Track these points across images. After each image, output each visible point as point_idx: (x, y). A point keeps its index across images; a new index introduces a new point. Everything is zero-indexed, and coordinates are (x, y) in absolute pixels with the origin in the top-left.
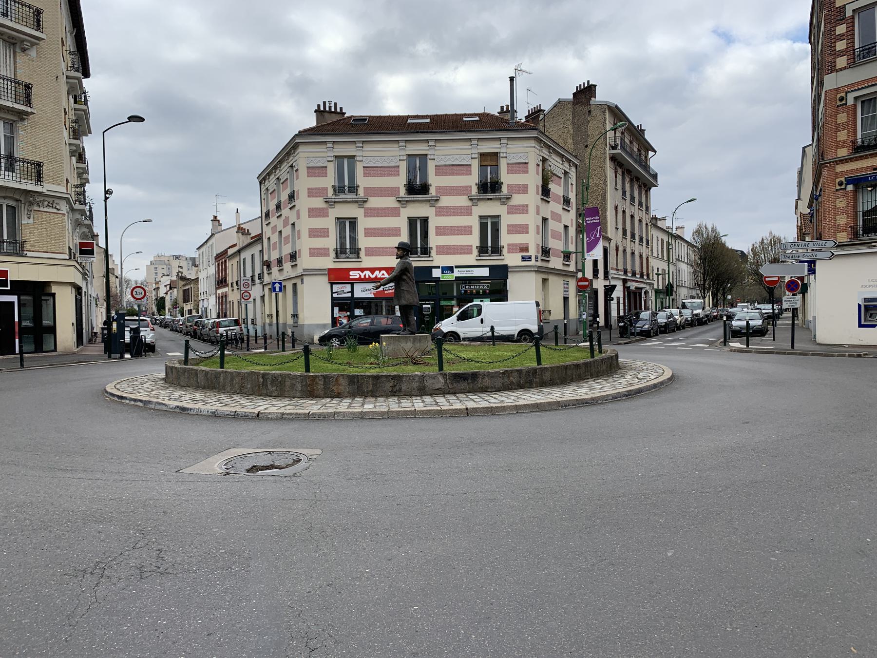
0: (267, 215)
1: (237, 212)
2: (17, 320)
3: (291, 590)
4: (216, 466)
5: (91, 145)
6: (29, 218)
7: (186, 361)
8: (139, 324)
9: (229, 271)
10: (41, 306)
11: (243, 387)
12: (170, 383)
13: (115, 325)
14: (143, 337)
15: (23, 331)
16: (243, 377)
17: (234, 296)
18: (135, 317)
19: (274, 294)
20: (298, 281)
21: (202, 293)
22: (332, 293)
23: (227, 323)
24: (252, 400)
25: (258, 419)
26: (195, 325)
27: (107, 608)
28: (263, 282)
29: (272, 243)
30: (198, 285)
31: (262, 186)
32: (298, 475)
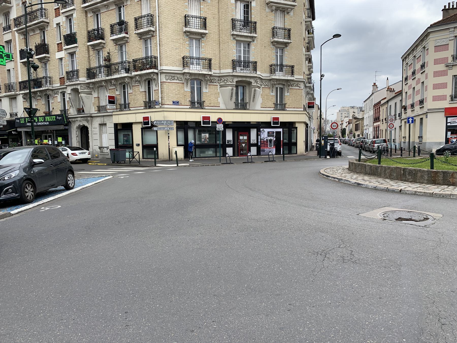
0: (406, 79)
1: (388, 79)
2: (282, 139)
3: (427, 288)
4: (378, 214)
5: (315, 54)
6: (288, 92)
7: (360, 160)
8: (334, 141)
9: (381, 113)
10: (292, 133)
11: (391, 175)
12: (351, 171)
13: (323, 142)
14: (336, 148)
15: (285, 144)
16: (392, 170)
17: (383, 126)
18: (332, 138)
19: (408, 125)
20: (424, 117)
21: (366, 126)
22: (447, 123)
23: (379, 141)
24: (397, 183)
25: (401, 193)
26: (362, 143)
27: (329, 272)
28: (401, 118)
29: (408, 95)
30: (363, 121)
31: (404, 62)
32: (428, 226)
